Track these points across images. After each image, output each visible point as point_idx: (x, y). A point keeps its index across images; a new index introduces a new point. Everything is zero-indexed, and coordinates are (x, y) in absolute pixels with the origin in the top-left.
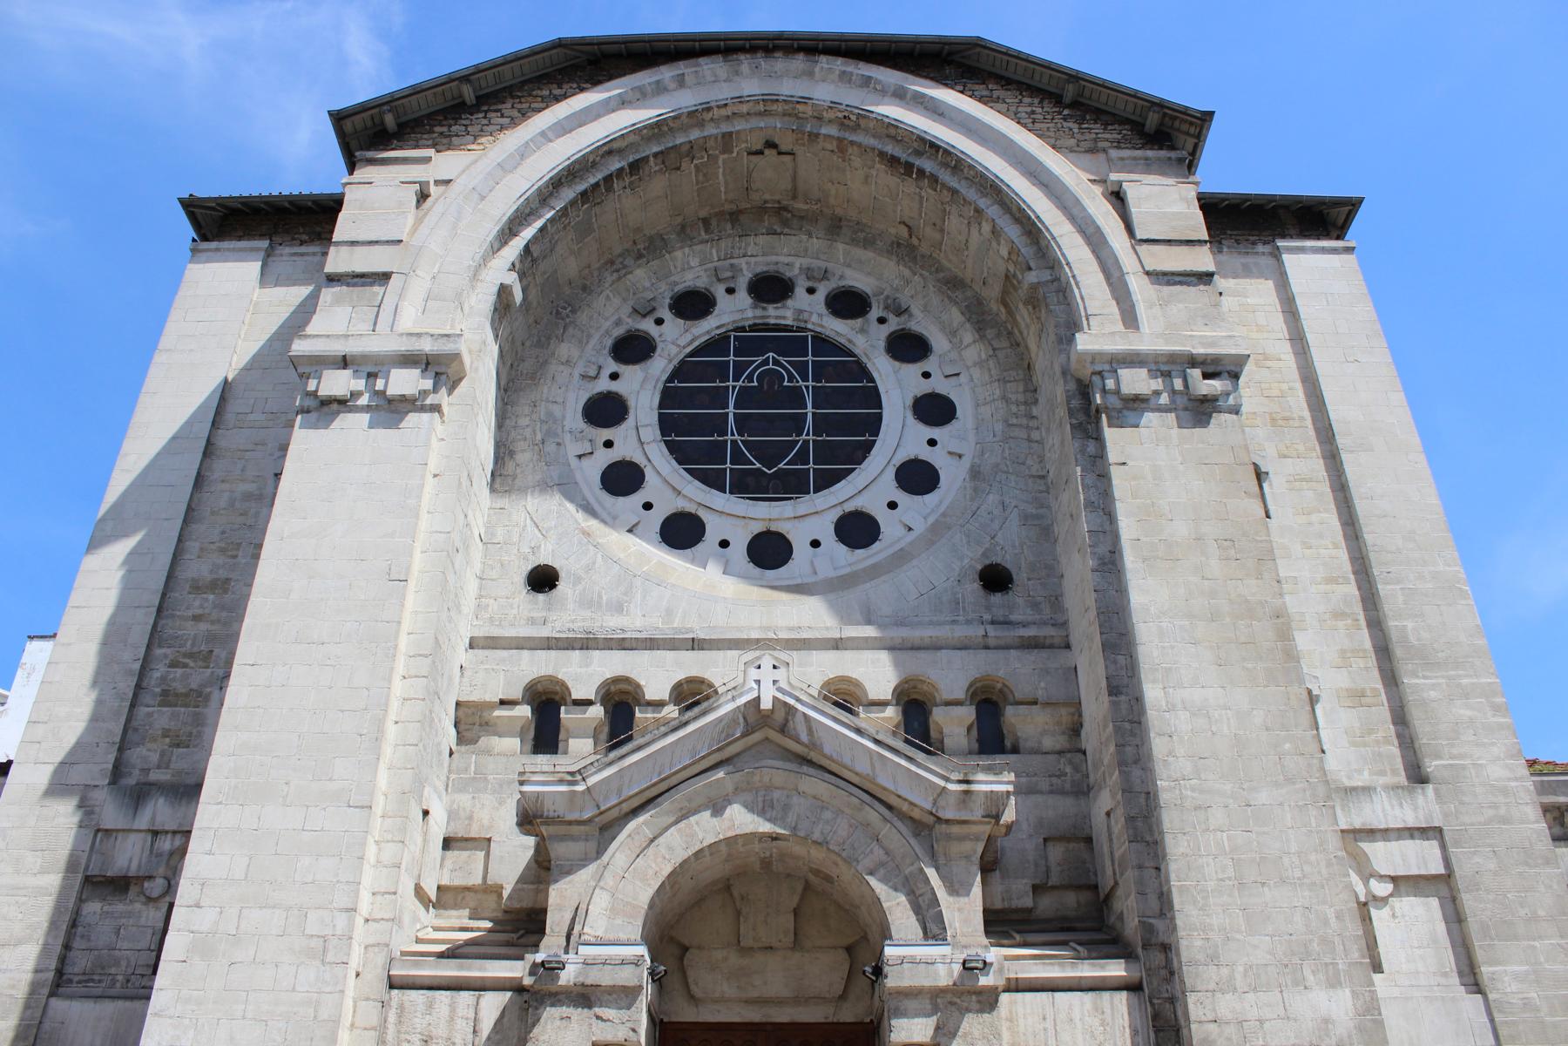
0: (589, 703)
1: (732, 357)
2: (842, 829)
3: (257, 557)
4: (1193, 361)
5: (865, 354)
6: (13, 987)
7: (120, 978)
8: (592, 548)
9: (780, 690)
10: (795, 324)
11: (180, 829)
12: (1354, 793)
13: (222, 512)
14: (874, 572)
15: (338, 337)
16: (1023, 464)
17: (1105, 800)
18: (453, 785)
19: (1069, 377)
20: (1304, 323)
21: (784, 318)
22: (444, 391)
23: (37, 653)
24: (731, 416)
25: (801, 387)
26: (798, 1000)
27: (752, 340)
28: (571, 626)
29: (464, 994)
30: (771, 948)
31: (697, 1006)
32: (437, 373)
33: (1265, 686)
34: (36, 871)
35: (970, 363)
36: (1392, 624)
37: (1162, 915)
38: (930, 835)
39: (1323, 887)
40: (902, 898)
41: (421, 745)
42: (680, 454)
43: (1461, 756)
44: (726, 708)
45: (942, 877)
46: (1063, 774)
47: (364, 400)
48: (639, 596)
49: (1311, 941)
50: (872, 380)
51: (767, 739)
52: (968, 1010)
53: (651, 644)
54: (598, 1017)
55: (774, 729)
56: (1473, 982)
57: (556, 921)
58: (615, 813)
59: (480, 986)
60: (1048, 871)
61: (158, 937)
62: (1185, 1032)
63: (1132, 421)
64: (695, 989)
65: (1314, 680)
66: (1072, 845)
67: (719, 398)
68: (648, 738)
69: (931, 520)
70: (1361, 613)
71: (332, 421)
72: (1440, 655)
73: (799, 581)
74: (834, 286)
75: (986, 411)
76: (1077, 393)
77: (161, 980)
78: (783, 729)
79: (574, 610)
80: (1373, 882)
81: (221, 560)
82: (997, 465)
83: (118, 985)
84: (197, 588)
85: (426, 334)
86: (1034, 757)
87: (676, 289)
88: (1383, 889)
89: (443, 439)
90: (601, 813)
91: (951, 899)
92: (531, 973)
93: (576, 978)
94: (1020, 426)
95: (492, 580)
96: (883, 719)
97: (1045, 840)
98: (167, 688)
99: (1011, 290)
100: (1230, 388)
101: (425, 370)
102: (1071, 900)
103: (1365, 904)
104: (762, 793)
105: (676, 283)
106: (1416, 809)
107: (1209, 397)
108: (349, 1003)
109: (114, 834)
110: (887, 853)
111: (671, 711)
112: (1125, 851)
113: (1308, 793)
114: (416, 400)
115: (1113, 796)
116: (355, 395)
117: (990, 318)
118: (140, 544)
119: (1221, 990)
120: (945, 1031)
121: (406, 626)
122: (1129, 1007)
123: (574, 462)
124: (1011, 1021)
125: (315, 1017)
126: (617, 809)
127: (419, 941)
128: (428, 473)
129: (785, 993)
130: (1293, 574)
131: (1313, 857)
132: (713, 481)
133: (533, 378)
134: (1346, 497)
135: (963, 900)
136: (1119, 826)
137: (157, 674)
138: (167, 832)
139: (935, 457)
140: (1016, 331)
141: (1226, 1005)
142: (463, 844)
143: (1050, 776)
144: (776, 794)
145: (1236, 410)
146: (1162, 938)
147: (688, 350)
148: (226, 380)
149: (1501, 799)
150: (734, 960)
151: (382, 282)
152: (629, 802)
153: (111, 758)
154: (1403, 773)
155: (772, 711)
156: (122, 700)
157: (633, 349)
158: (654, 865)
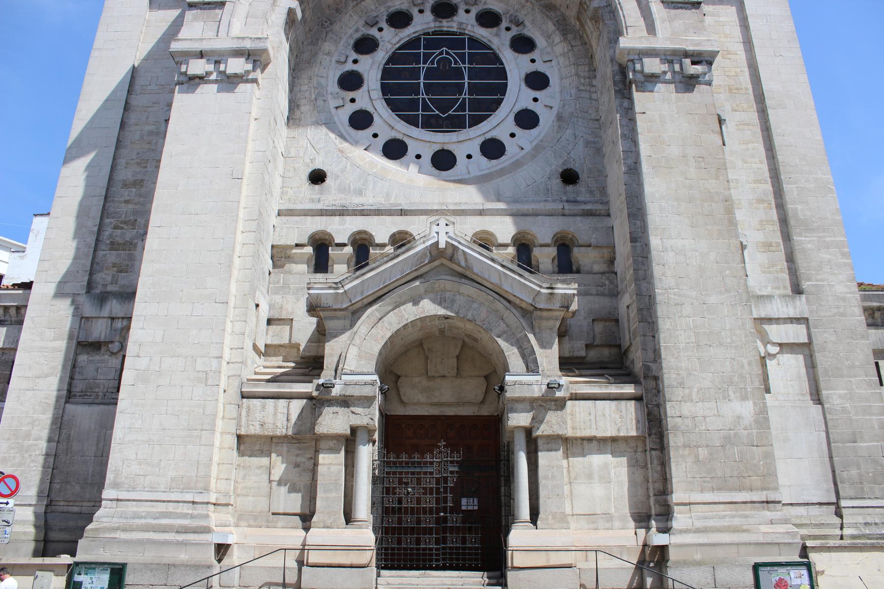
0: (344, 245)
1: (422, 50)
2: (483, 313)
3: (158, 167)
4: (686, 54)
5: (498, 48)
6: (46, 398)
7: (100, 394)
8: (344, 159)
9: (449, 237)
10: (459, 31)
11: (126, 316)
12: (762, 299)
13: (137, 142)
14: (501, 172)
15: (197, 40)
16: (587, 112)
17: (626, 299)
18: (272, 290)
19: (614, 63)
20: (752, 32)
21: (452, 27)
22: (259, 71)
23: (40, 224)
24: (422, 84)
25: (461, 67)
26: (458, 404)
27: (434, 40)
28: (334, 203)
29: (281, 401)
30: (444, 376)
31: (405, 407)
32: (254, 61)
33: (717, 239)
34: (52, 339)
35: (558, 54)
36: (790, 206)
37: (655, 361)
38: (531, 317)
39: (742, 348)
40: (515, 350)
41: (253, 269)
42: (393, 106)
43: (822, 280)
44: (420, 248)
45: (537, 339)
46: (604, 285)
47: (213, 77)
48: (371, 186)
49: (734, 376)
50: (502, 64)
51: (442, 264)
52: (550, 409)
53: (378, 212)
54: (353, 412)
55: (446, 259)
56: (817, 398)
57: (329, 362)
58: (359, 305)
59: (290, 397)
60: (594, 338)
61: (118, 372)
62: (664, 422)
63: (650, 89)
64: (404, 398)
65: (744, 237)
66: (607, 323)
67: (415, 74)
68: (377, 264)
69: (534, 144)
70: (773, 200)
71: (196, 89)
72: (815, 224)
73: (460, 177)
74: (481, 8)
75: (566, 82)
76: (619, 72)
77: (121, 395)
78: (451, 259)
79: (335, 194)
80: (769, 346)
81: (138, 169)
82: (572, 113)
83: (100, 397)
84: (125, 185)
85: (247, 37)
86: (588, 275)
87: (391, 10)
88: (773, 350)
89: (259, 99)
90: (352, 305)
91: (542, 351)
92: (317, 390)
93: (341, 392)
94: (586, 91)
95: (289, 178)
96: (506, 254)
97: (593, 320)
98: (112, 240)
99: (583, 11)
100: (707, 70)
101: (247, 59)
102: (606, 353)
103: (764, 358)
104: (440, 293)
105: (390, 7)
106: (795, 308)
107: (694, 76)
108: (221, 406)
109: (91, 320)
110: (507, 326)
111: (390, 249)
112: (636, 327)
113: (737, 298)
114: (243, 76)
115: (631, 297)
116: (208, 74)
117: (570, 28)
118: (93, 160)
119: (684, 401)
120: (537, 420)
121: (242, 204)
122: (636, 409)
123: (333, 111)
124: (572, 415)
125: (203, 413)
126: (361, 302)
127: (256, 373)
128: (252, 118)
129: (452, 400)
130: (735, 178)
131: (738, 332)
132: (412, 121)
133: (309, 63)
134: (769, 135)
135: (549, 351)
136: (634, 313)
137: (107, 233)
138: (119, 318)
139: (537, 108)
140: (585, 35)
141: (687, 409)
142: (278, 322)
143: (597, 286)
144: (447, 294)
145: (709, 83)
146: (655, 373)
147: (398, 46)
148: (134, 66)
149: (842, 303)
150: (425, 382)
151: (220, 7)
152: (368, 298)
153: (86, 278)
154: (790, 288)
155: (445, 249)
156: (89, 247)
157: (365, 45)
158: (381, 333)
